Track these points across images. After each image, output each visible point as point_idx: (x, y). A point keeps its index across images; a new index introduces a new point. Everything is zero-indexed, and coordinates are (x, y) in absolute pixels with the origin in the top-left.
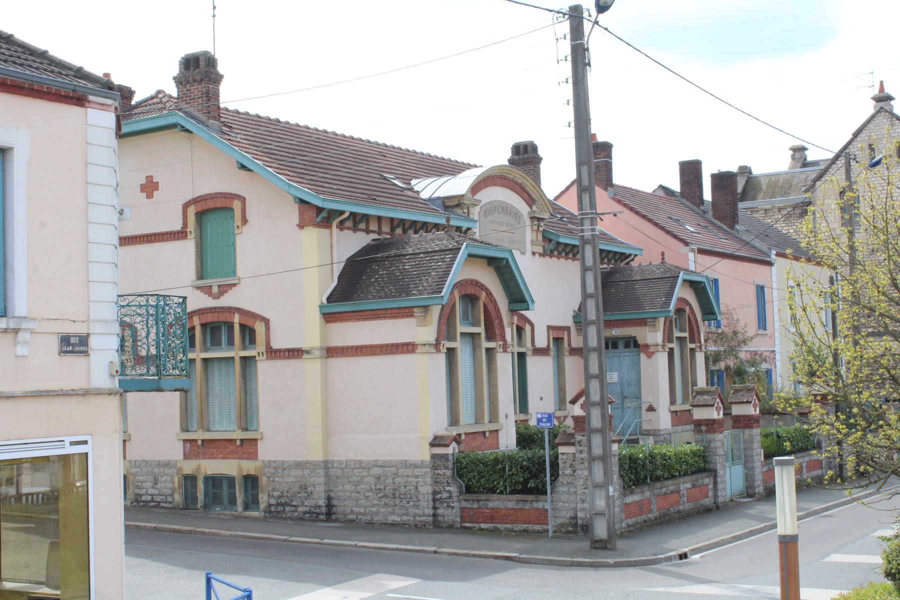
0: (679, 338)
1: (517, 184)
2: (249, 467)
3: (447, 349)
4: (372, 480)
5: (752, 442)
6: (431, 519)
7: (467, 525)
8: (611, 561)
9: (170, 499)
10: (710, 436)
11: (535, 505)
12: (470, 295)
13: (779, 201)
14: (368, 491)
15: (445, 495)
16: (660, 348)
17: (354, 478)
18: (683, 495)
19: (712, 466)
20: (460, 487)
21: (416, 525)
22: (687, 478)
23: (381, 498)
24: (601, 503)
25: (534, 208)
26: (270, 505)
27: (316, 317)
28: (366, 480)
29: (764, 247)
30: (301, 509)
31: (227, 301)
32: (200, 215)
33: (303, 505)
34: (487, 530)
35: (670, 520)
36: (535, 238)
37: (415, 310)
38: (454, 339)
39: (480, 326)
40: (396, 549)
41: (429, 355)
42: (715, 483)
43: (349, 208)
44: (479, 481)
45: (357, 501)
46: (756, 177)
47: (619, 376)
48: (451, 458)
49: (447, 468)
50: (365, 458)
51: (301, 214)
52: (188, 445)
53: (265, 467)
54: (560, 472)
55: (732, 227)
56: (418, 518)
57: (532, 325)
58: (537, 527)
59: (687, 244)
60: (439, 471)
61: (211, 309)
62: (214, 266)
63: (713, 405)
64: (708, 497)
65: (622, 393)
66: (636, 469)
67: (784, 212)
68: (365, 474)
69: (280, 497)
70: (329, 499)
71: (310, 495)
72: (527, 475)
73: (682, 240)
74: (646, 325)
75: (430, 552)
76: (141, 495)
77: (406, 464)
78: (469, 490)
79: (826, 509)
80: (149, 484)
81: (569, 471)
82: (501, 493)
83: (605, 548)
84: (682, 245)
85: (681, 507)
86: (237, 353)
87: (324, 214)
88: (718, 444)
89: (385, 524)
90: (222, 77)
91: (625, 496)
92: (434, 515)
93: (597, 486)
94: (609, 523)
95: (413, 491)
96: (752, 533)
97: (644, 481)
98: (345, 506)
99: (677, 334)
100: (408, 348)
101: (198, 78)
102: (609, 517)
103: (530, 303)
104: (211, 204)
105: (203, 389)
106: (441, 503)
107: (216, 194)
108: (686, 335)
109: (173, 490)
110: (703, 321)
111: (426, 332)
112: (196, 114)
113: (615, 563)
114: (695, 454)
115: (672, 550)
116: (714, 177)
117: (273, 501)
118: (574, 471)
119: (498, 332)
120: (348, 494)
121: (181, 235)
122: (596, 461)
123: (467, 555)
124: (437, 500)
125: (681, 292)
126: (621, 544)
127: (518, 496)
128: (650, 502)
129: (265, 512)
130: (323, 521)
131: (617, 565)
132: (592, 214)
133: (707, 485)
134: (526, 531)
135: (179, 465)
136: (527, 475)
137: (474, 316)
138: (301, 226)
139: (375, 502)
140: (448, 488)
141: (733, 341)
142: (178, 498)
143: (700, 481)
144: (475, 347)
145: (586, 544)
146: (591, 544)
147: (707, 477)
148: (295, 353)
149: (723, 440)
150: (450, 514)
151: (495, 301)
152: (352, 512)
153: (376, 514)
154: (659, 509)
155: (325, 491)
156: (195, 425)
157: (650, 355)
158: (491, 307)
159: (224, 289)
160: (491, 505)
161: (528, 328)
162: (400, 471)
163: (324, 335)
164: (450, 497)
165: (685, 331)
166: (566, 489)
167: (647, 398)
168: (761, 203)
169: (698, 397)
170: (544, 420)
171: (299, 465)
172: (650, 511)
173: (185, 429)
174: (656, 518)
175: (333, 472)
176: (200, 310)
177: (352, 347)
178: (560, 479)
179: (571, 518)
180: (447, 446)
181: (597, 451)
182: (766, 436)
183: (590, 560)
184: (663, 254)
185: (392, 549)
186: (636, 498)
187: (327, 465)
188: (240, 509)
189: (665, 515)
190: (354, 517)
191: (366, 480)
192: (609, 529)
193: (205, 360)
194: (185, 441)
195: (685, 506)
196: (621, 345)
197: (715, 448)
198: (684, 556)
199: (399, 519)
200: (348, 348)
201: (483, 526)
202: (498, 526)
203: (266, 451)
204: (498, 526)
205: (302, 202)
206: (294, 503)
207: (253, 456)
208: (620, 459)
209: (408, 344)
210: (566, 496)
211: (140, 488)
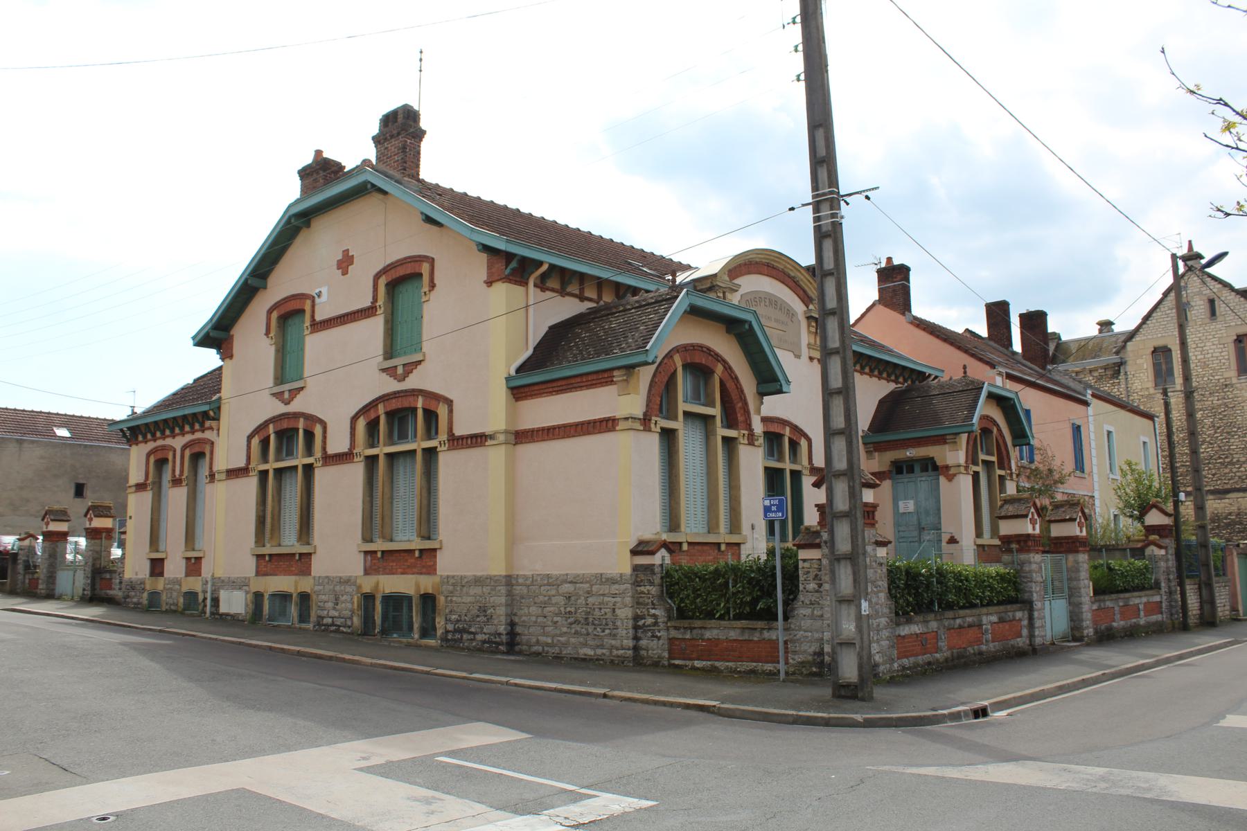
0: (984, 462)
1: (789, 276)
2: (426, 583)
3: (662, 429)
4: (561, 600)
5: (1077, 570)
6: (630, 652)
7: (677, 662)
8: (859, 717)
9: (349, 623)
10: (1023, 556)
11: (766, 635)
12: (700, 366)
13: (1090, 363)
14: (557, 615)
15: (650, 621)
16: (962, 469)
17: (541, 598)
18: (987, 630)
19: (1026, 596)
20: (669, 610)
21: (612, 661)
22: (991, 609)
23: (571, 624)
24: (849, 627)
25: (811, 307)
26: (447, 632)
27: (499, 393)
28: (554, 600)
29: (1079, 387)
30: (479, 637)
31: (412, 382)
32: (393, 286)
33: (482, 632)
34: (703, 670)
35: (963, 664)
36: (812, 341)
37: (616, 373)
38: (675, 418)
39: (714, 407)
40: (556, 690)
41: (631, 433)
42: (1031, 618)
43: (549, 259)
44: (693, 602)
45: (544, 627)
46: (1066, 343)
47: (916, 504)
48: (657, 570)
49: (651, 583)
50: (555, 572)
51: (490, 267)
52: (369, 558)
53: (442, 583)
54: (801, 587)
55: (1044, 368)
56: (615, 652)
57: (809, 441)
58: (769, 667)
59: (993, 366)
60: (642, 588)
61: (395, 393)
62: (399, 345)
63: (1026, 516)
64: (1021, 636)
65: (919, 524)
66: (917, 589)
67: (1096, 374)
68: (553, 592)
69: (458, 621)
70: (512, 624)
71: (490, 619)
72: (757, 593)
73: (987, 363)
74: (945, 443)
75: (597, 696)
76: (323, 618)
77: (603, 579)
78: (682, 614)
79: (1181, 657)
80: (330, 605)
81: (812, 586)
82: (721, 618)
83: (854, 697)
84: (988, 368)
85: (984, 648)
86: (419, 444)
87: (514, 264)
88: (1034, 566)
89: (576, 659)
90: (423, 133)
91: (898, 624)
92: (636, 649)
93: (842, 601)
94: (860, 657)
95: (609, 615)
96: (1085, 683)
97: (929, 608)
98: (531, 635)
99: (982, 457)
100: (606, 425)
101: (395, 132)
102: (862, 648)
103: (783, 382)
104: (401, 272)
105: (386, 490)
106: (645, 632)
107: (405, 258)
108: (994, 459)
109: (352, 611)
110: (1015, 446)
111: (628, 401)
112: (391, 172)
113: (866, 720)
114: (1002, 578)
115: (963, 704)
116: (1022, 316)
117: (450, 627)
118: (820, 585)
119: (741, 418)
120: (534, 619)
121: (368, 312)
122: (843, 563)
123: (646, 702)
124: (640, 627)
125: (983, 408)
126: (879, 692)
127: (744, 623)
128: (936, 637)
129: (442, 640)
130: (503, 653)
131: (869, 724)
132: (831, 193)
133: (1020, 620)
134: (753, 672)
135: (358, 581)
136: (757, 593)
137: (707, 395)
138: (489, 283)
139: (565, 629)
140: (653, 611)
141: (1047, 480)
142: (356, 621)
143: (1010, 614)
144: (708, 435)
145: (827, 692)
146: (843, 694)
147: (1020, 610)
148: (478, 440)
149: (1039, 565)
150: (655, 647)
151: (737, 378)
152: (538, 642)
153: (565, 644)
154: (950, 648)
155: (507, 615)
156: (376, 533)
157: (950, 478)
158: (730, 385)
159: (410, 368)
160: (708, 635)
161: (804, 443)
162: (595, 588)
163: (511, 415)
164: (656, 624)
165: (992, 455)
166: (807, 611)
167: (947, 528)
168: (1071, 366)
169: (1006, 507)
170: (774, 508)
171: (478, 581)
172: (937, 650)
173: (367, 539)
174: (946, 660)
175: (518, 590)
176: (384, 396)
177: (543, 429)
178: (801, 597)
179: (815, 653)
180: (652, 553)
181: (844, 546)
182: (1095, 568)
183: (825, 715)
184: (965, 367)
185: (551, 690)
186: (916, 629)
187: (509, 581)
188: (416, 636)
189: (960, 656)
190: (540, 649)
191: (554, 600)
192: (860, 667)
193: (391, 456)
194: (366, 553)
195: (990, 647)
196: (917, 468)
197: (1030, 571)
198: (981, 713)
199: (592, 653)
200: (538, 430)
201: (698, 664)
202: (717, 664)
203: (446, 564)
204: (717, 664)
205: (486, 248)
206: (473, 630)
207: (431, 570)
208: (889, 572)
209: (607, 420)
210: (809, 622)
211: (323, 609)
